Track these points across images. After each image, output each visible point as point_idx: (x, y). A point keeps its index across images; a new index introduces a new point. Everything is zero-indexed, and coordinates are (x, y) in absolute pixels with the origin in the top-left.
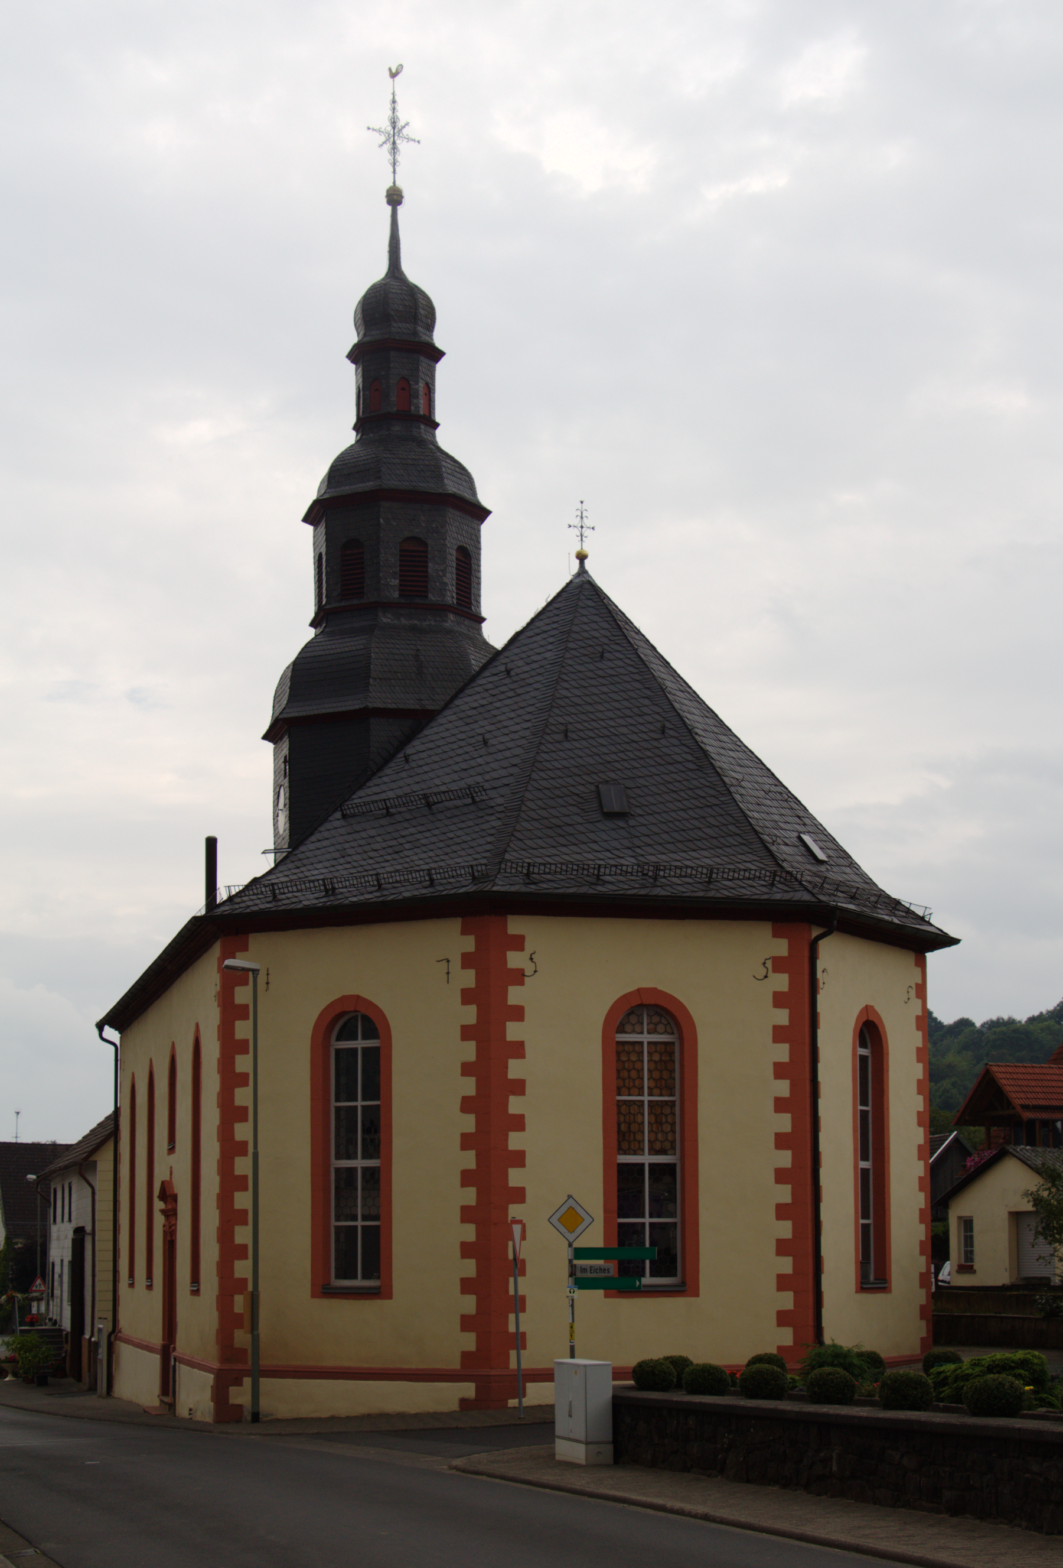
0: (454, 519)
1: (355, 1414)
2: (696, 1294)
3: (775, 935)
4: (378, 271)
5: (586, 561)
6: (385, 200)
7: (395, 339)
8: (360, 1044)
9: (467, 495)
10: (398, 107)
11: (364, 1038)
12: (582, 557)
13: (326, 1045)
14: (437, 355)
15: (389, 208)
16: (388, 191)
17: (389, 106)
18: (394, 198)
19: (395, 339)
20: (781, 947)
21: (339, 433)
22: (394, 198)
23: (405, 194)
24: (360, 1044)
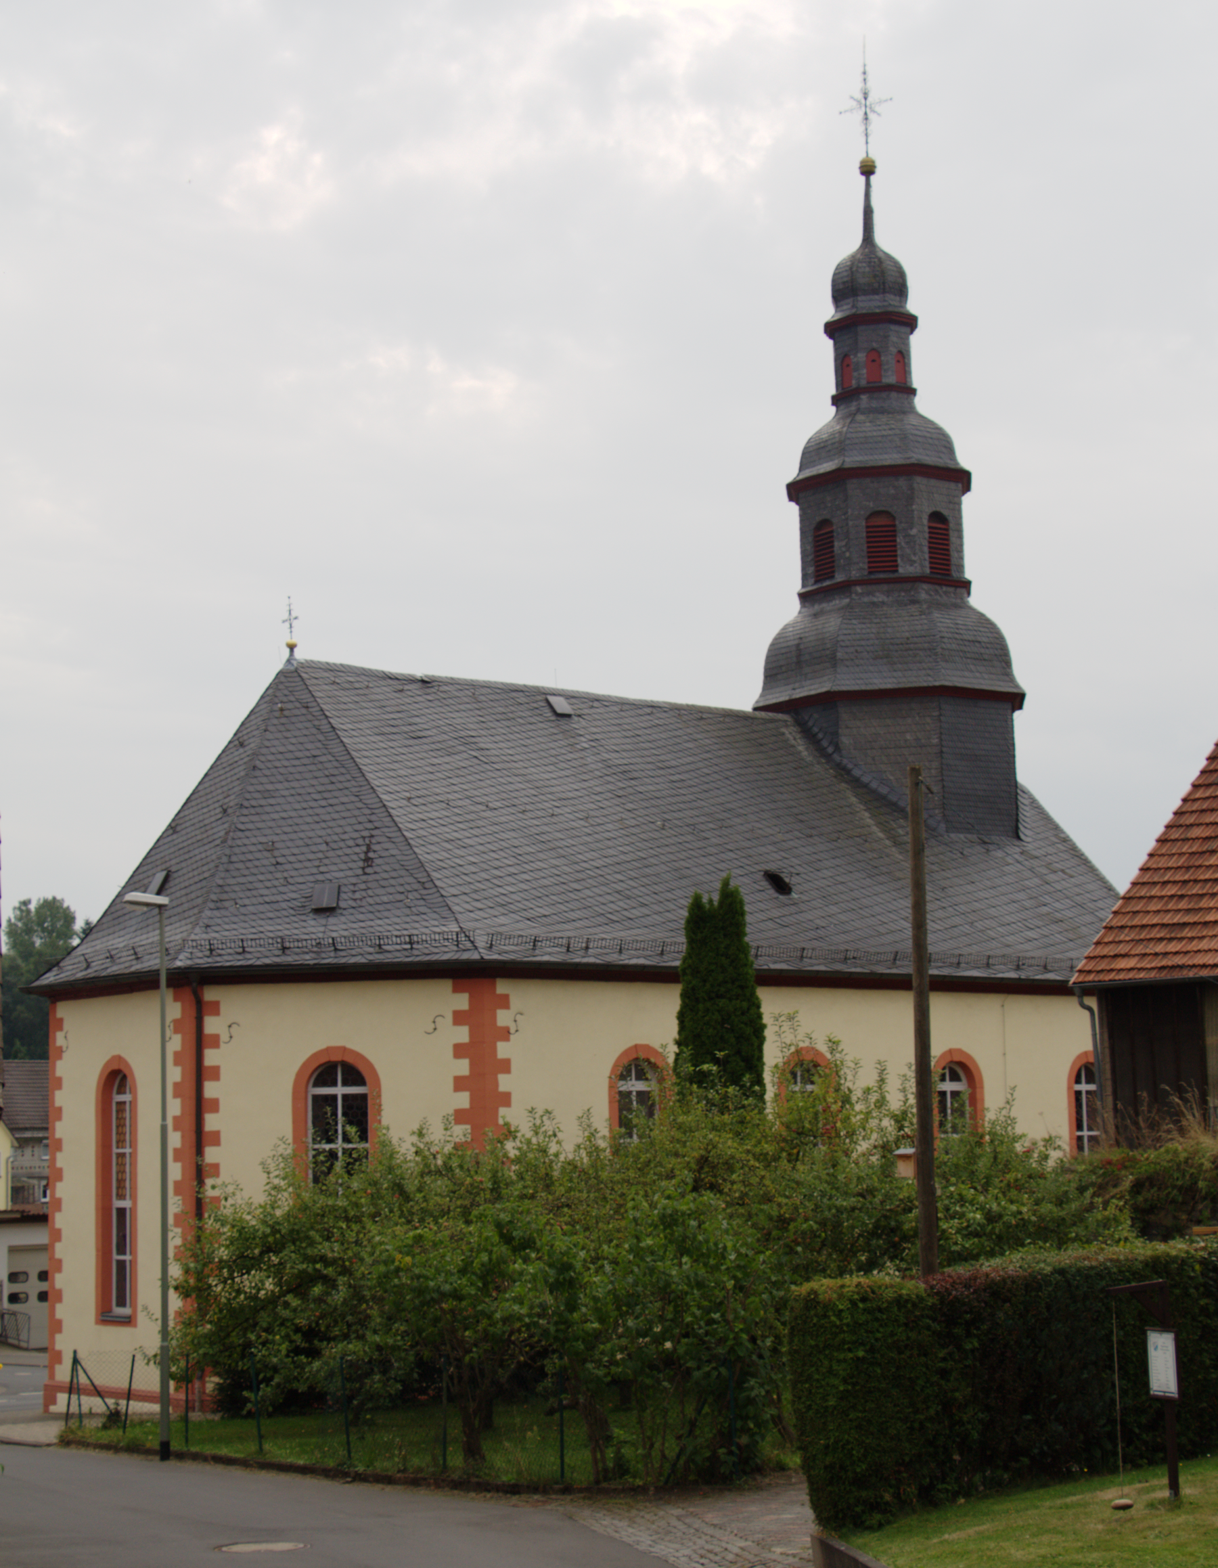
0: (927, 496)
1: (294, 1475)
2: (135, 1326)
3: (456, 990)
4: (852, 243)
5: (296, 650)
6: (858, 171)
7: (870, 312)
8: (340, 1090)
9: (951, 465)
10: (870, 77)
11: (345, 1084)
12: (292, 647)
13: (306, 1092)
14: (910, 323)
15: (863, 178)
16: (862, 162)
17: (861, 78)
18: (868, 170)
19: (870, 312)
20: (462, 1001)
21: (815, 411)
22: (868, 170)
23: (878, 164)
24: (340, 1090)
